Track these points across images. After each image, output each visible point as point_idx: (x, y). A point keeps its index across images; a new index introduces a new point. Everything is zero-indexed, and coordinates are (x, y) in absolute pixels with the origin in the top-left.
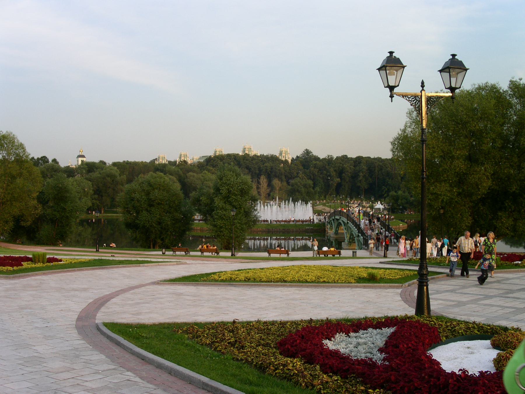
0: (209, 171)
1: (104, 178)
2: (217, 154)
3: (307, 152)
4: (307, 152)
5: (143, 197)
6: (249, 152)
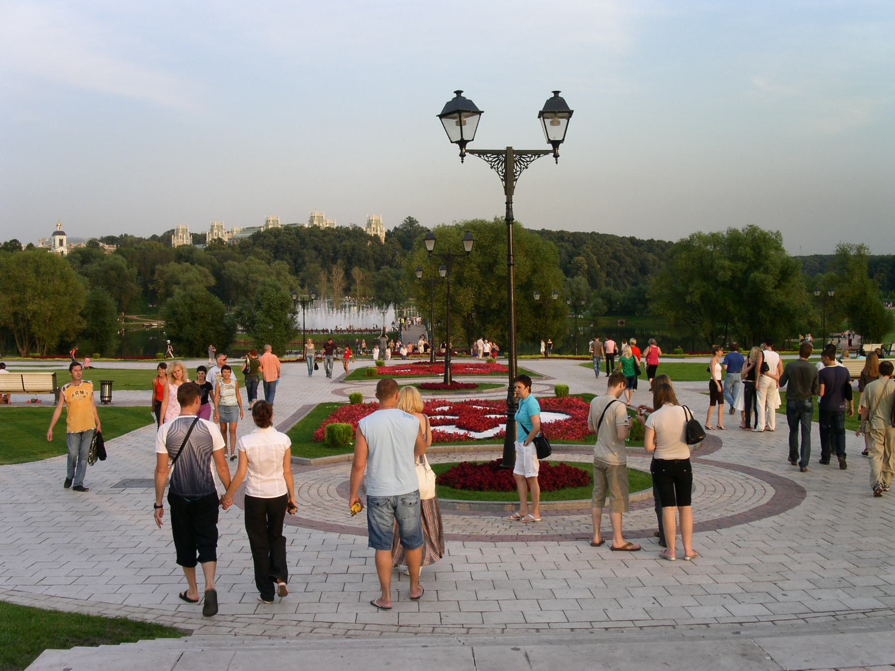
0: (256, 254)
1: (106, 272)
2: (270, 227)
3: (410, 221)
4: (411, 222)
5: (187, 311)
6: (319, 224)
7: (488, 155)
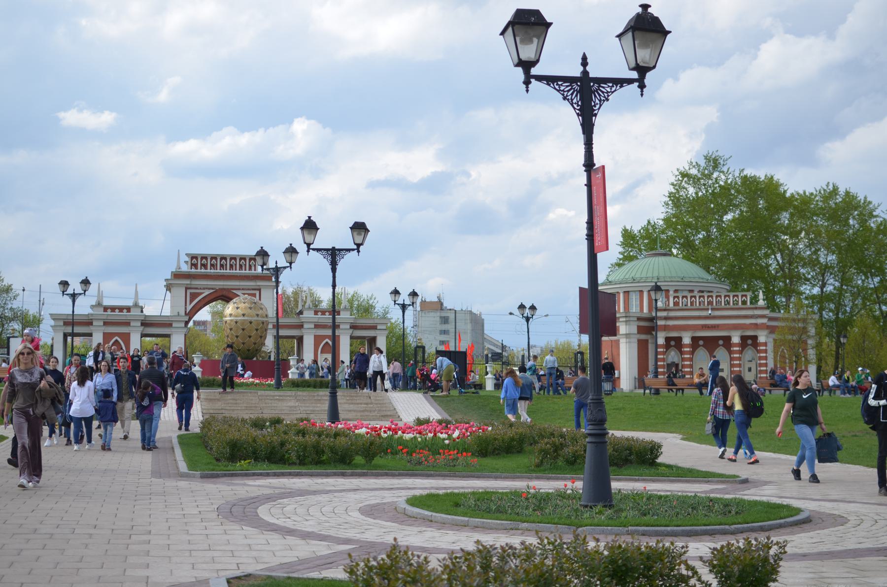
7: (560, 83)
